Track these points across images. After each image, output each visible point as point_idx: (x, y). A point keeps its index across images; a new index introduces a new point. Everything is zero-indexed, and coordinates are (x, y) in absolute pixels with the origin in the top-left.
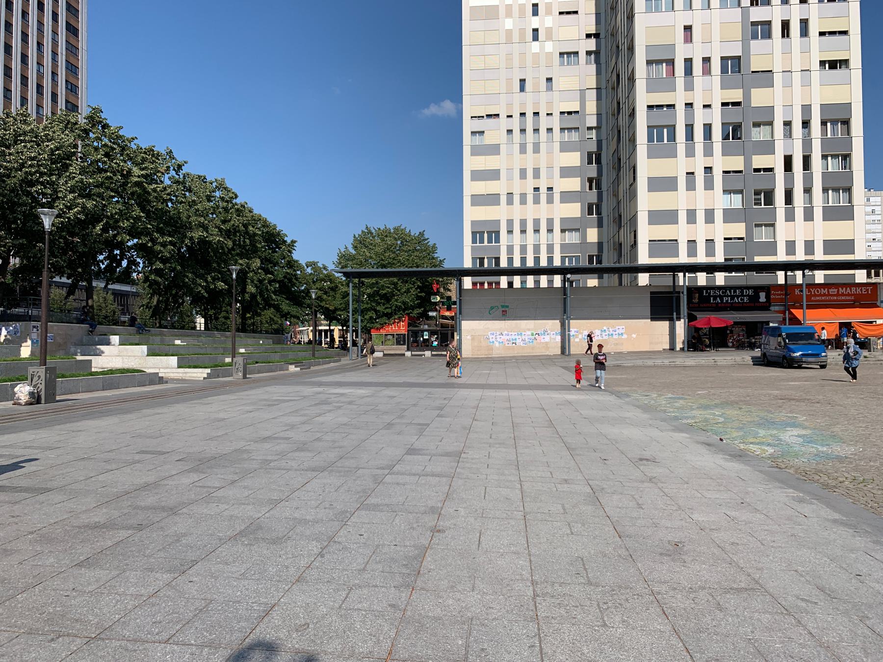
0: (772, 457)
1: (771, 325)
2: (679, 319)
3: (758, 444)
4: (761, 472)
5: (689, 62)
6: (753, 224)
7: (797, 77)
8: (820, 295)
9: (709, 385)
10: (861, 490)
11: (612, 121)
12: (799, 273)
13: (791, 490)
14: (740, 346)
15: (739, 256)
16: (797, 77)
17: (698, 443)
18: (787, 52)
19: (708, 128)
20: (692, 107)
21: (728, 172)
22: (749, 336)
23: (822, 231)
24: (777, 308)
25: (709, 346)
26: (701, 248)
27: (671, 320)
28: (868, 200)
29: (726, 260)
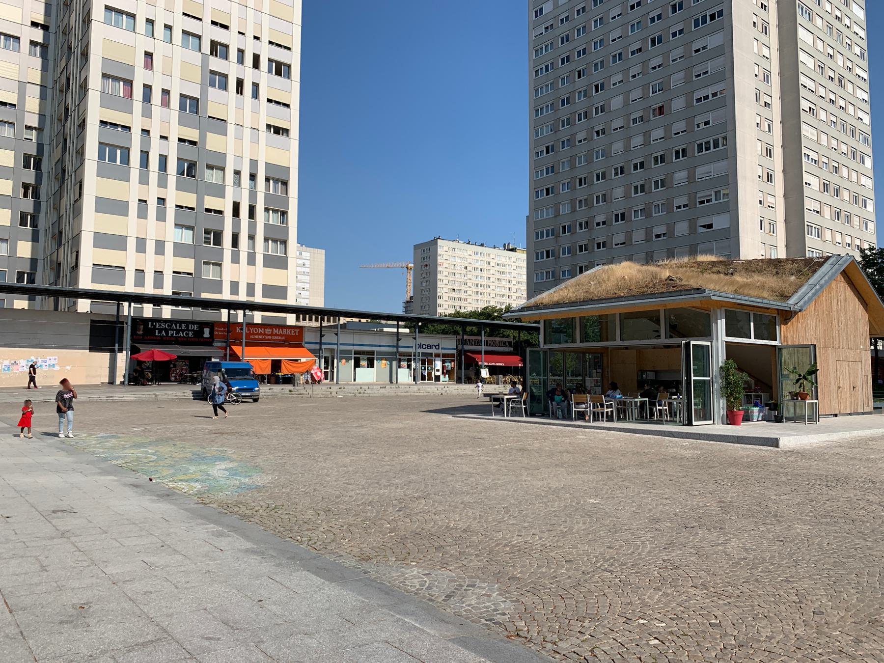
0: (199, 494)
1: (213, 360)
2: (121, 351)
3: (187, 481)
4: (186, 510)
5: (147, 88)
6: (203, 262)
7: (247, 132)
8: (258, 334)
9: (146, 421)
10: (271, 516)
11: (57, 127)
12: (240, 313)
13: (212, 525)
14: (182, 380)
15: (187, 291)
16: (247, 132)
17: (125, 485)
18: (240, 108)
19: (163, 159)
20: (148, 134)
21: (181, 207)
22: (192, 371)
23: (262, 276)
24: (219, 344)
25: (151, 380)
26: (149, 278)
27: (112, 351)
28: (301, 254)
29: (174, 293)
